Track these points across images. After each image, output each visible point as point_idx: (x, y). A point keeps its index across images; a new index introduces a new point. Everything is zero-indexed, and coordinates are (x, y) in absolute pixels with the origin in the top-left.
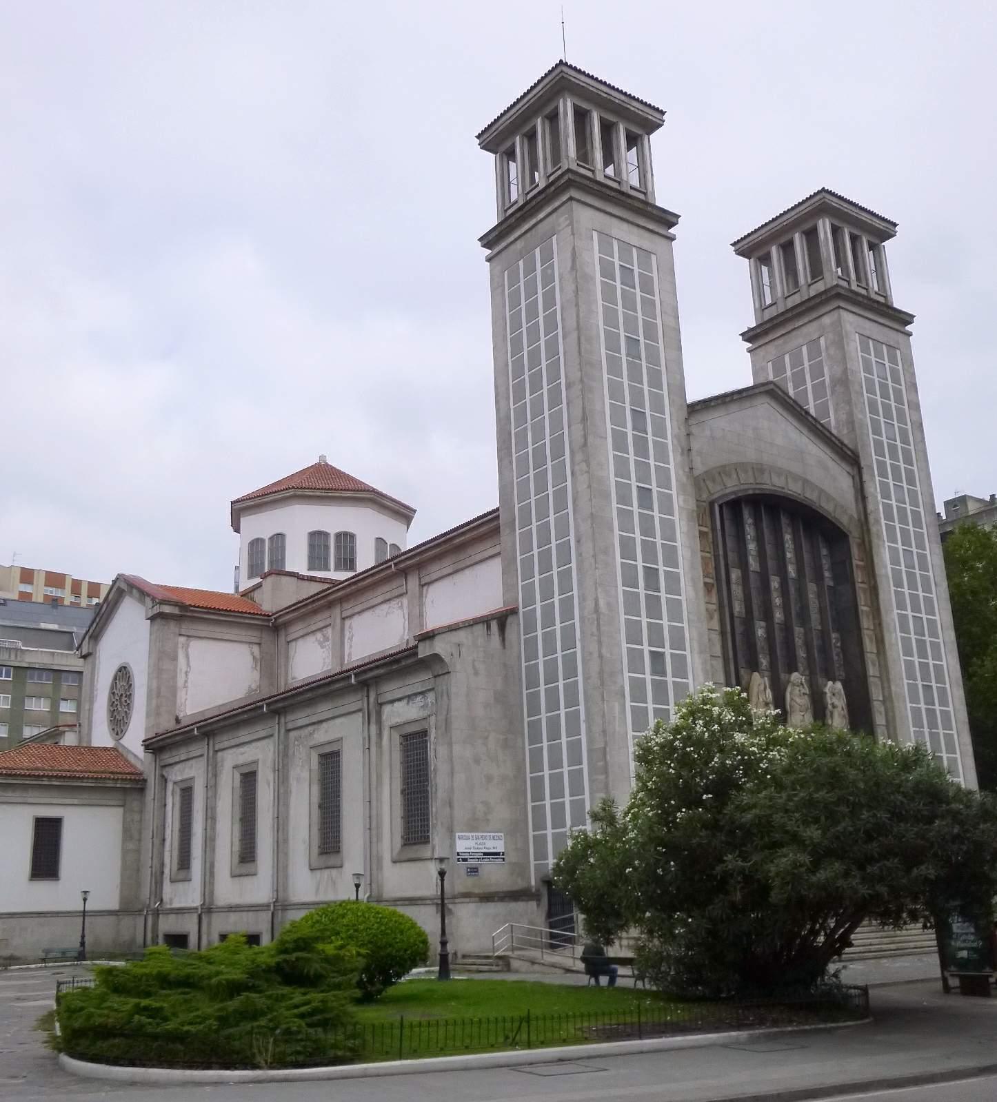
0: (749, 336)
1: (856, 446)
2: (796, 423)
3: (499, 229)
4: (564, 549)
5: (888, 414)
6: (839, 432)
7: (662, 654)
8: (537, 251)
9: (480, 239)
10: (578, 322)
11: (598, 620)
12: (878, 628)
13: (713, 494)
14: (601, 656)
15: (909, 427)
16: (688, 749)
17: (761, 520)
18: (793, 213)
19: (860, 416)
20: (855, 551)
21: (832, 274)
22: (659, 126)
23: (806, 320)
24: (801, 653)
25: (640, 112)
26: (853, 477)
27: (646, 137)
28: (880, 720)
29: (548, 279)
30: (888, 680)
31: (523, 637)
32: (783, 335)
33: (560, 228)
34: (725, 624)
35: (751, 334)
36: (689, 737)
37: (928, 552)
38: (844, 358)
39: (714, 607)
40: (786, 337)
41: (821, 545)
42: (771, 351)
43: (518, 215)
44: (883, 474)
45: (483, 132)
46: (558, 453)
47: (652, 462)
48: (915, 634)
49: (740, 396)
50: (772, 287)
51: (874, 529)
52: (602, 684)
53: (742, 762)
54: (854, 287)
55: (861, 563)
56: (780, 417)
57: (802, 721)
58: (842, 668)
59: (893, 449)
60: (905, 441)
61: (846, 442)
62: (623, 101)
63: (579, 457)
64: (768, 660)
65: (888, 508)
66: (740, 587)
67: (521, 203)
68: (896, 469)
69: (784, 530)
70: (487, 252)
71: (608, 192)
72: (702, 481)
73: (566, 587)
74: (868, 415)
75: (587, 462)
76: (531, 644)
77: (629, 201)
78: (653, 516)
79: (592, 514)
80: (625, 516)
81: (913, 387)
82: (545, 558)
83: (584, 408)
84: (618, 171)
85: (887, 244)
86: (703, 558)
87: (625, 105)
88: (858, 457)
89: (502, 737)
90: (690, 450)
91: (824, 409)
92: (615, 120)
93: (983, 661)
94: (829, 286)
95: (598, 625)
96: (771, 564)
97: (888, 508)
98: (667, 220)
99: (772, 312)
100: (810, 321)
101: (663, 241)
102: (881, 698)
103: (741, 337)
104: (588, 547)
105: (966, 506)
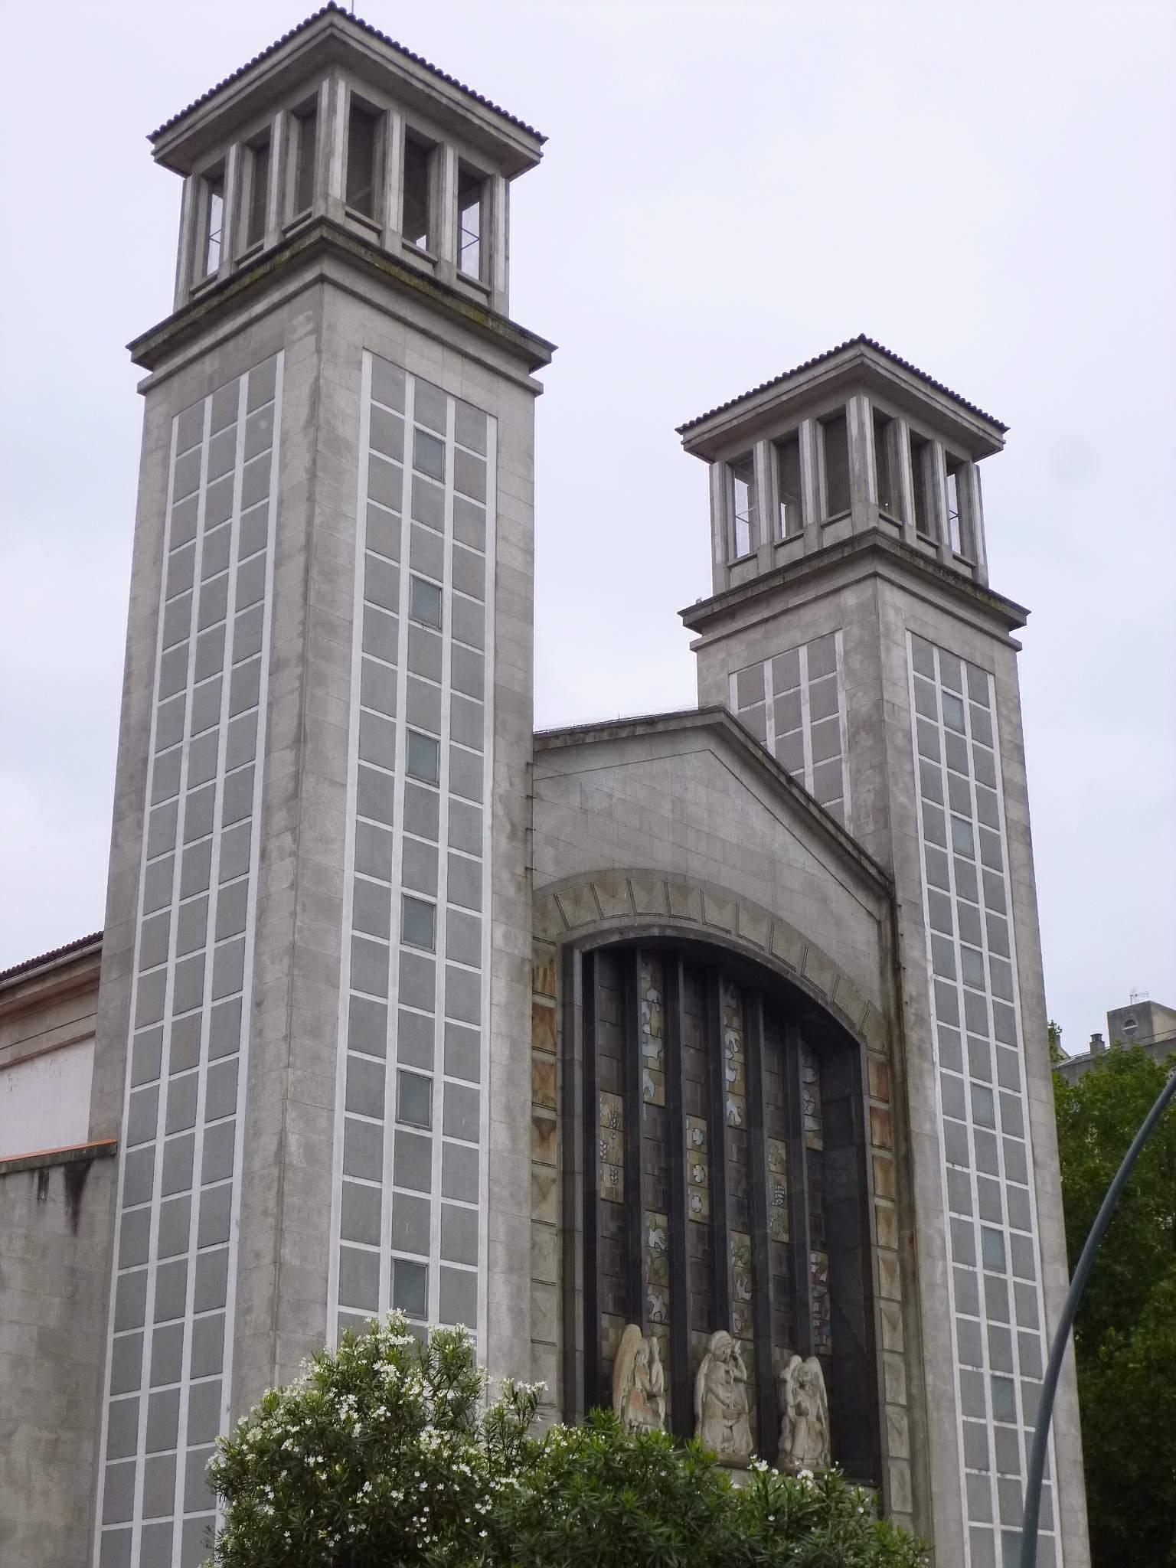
0: (698, 618)
1: (889, 862)
2: (766, 800)
3: (173, 328)
4: (227, 1020)
5: (960, 802)
6: (858, 827)
7: (422, 1269)
8: (244, 380)
9: (132, 346)
10: (309, 537)
11: (281, 1180)
12: (907, 1247)
13: (572, 928)
14: (278, 1262)
15: (1002, 833)
16: (312, 1460)
17: (676, 997)
18: (802, 379)
19: (903, 799)
20: (871, 1079)
21: (865, 513)
22: (532, 163)
23: (811, 594)
24: (741, 1292)
25: (493, 131)
26: (879, 923)
27: (502, 181)
28: (897, 1447)
29: (259, 440)
30: (921, 1362)
31: (120, 1212)
32: (766, 621)
33: (295, 337)
34: (573, 1214)
35: (702, 613)
36: (321, 1433)
37: (1023, 1095)
38: (879, 679)
39: (552, 1173)
40: (771, 625)
41: (801, 1060)
42: (738, 651)
43: (214, 302)
44: (941, 923)
45: (164, 130)
46: (238, 811)
47: (442, 847)
48: (985, 1266)
49: (649, 730)
50: (753, 523)
51: (913, 1036)
52: (275, 1326)
53: (427, 1497)
54: (911, 539)
55: (883, 1106)
56: (732, 781)
57: (725, 1440)
58: (827, 1329)
59: (966, 874)
60: (992, 859)
61: (870, 850)
62: (458, 104)
63: (280, 819)
64: (667, 1301)
65: (946, 997)
66: (618, 1136)
67: (224, 276)
68: (969, 917)
69: (724, 1021)
70: (143, 373)
71: (405, 277)
72: (551, 899)
73: (221, 1104)
74: (919, 799)
75: (295, 831)
76: (136, 1226)
77: (448, 301)
78: (433, 963)
79: (293, 946)
80: (370, 957)
81: (1016, 752)
82: (187, 1035)
83: (301, 716)
84: (434, 244)
85: (986, 465)
86: (534, 1062)
87: (461, 111)
88: (892, 883)
89: (45, 1435)
90: (529, 830)
91: (830, 779)
92: (489, 170)
93: (1128, 1336)
94: (860, 529)
95: (281, 1193)
96: (689, 1091)
97: (946, 997)
98: (1010, 616)
99: (749, 572)
100: (818, 599)
101: (516, 394)
102: (903, 1400)
103: (129, 353)
104: (277, 1016)
105: (1150, 1023)
